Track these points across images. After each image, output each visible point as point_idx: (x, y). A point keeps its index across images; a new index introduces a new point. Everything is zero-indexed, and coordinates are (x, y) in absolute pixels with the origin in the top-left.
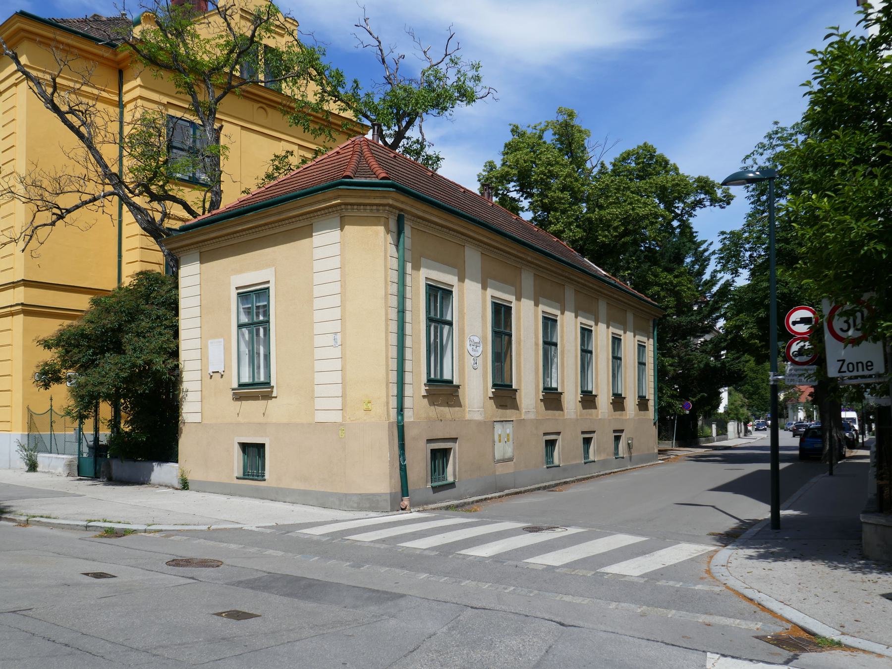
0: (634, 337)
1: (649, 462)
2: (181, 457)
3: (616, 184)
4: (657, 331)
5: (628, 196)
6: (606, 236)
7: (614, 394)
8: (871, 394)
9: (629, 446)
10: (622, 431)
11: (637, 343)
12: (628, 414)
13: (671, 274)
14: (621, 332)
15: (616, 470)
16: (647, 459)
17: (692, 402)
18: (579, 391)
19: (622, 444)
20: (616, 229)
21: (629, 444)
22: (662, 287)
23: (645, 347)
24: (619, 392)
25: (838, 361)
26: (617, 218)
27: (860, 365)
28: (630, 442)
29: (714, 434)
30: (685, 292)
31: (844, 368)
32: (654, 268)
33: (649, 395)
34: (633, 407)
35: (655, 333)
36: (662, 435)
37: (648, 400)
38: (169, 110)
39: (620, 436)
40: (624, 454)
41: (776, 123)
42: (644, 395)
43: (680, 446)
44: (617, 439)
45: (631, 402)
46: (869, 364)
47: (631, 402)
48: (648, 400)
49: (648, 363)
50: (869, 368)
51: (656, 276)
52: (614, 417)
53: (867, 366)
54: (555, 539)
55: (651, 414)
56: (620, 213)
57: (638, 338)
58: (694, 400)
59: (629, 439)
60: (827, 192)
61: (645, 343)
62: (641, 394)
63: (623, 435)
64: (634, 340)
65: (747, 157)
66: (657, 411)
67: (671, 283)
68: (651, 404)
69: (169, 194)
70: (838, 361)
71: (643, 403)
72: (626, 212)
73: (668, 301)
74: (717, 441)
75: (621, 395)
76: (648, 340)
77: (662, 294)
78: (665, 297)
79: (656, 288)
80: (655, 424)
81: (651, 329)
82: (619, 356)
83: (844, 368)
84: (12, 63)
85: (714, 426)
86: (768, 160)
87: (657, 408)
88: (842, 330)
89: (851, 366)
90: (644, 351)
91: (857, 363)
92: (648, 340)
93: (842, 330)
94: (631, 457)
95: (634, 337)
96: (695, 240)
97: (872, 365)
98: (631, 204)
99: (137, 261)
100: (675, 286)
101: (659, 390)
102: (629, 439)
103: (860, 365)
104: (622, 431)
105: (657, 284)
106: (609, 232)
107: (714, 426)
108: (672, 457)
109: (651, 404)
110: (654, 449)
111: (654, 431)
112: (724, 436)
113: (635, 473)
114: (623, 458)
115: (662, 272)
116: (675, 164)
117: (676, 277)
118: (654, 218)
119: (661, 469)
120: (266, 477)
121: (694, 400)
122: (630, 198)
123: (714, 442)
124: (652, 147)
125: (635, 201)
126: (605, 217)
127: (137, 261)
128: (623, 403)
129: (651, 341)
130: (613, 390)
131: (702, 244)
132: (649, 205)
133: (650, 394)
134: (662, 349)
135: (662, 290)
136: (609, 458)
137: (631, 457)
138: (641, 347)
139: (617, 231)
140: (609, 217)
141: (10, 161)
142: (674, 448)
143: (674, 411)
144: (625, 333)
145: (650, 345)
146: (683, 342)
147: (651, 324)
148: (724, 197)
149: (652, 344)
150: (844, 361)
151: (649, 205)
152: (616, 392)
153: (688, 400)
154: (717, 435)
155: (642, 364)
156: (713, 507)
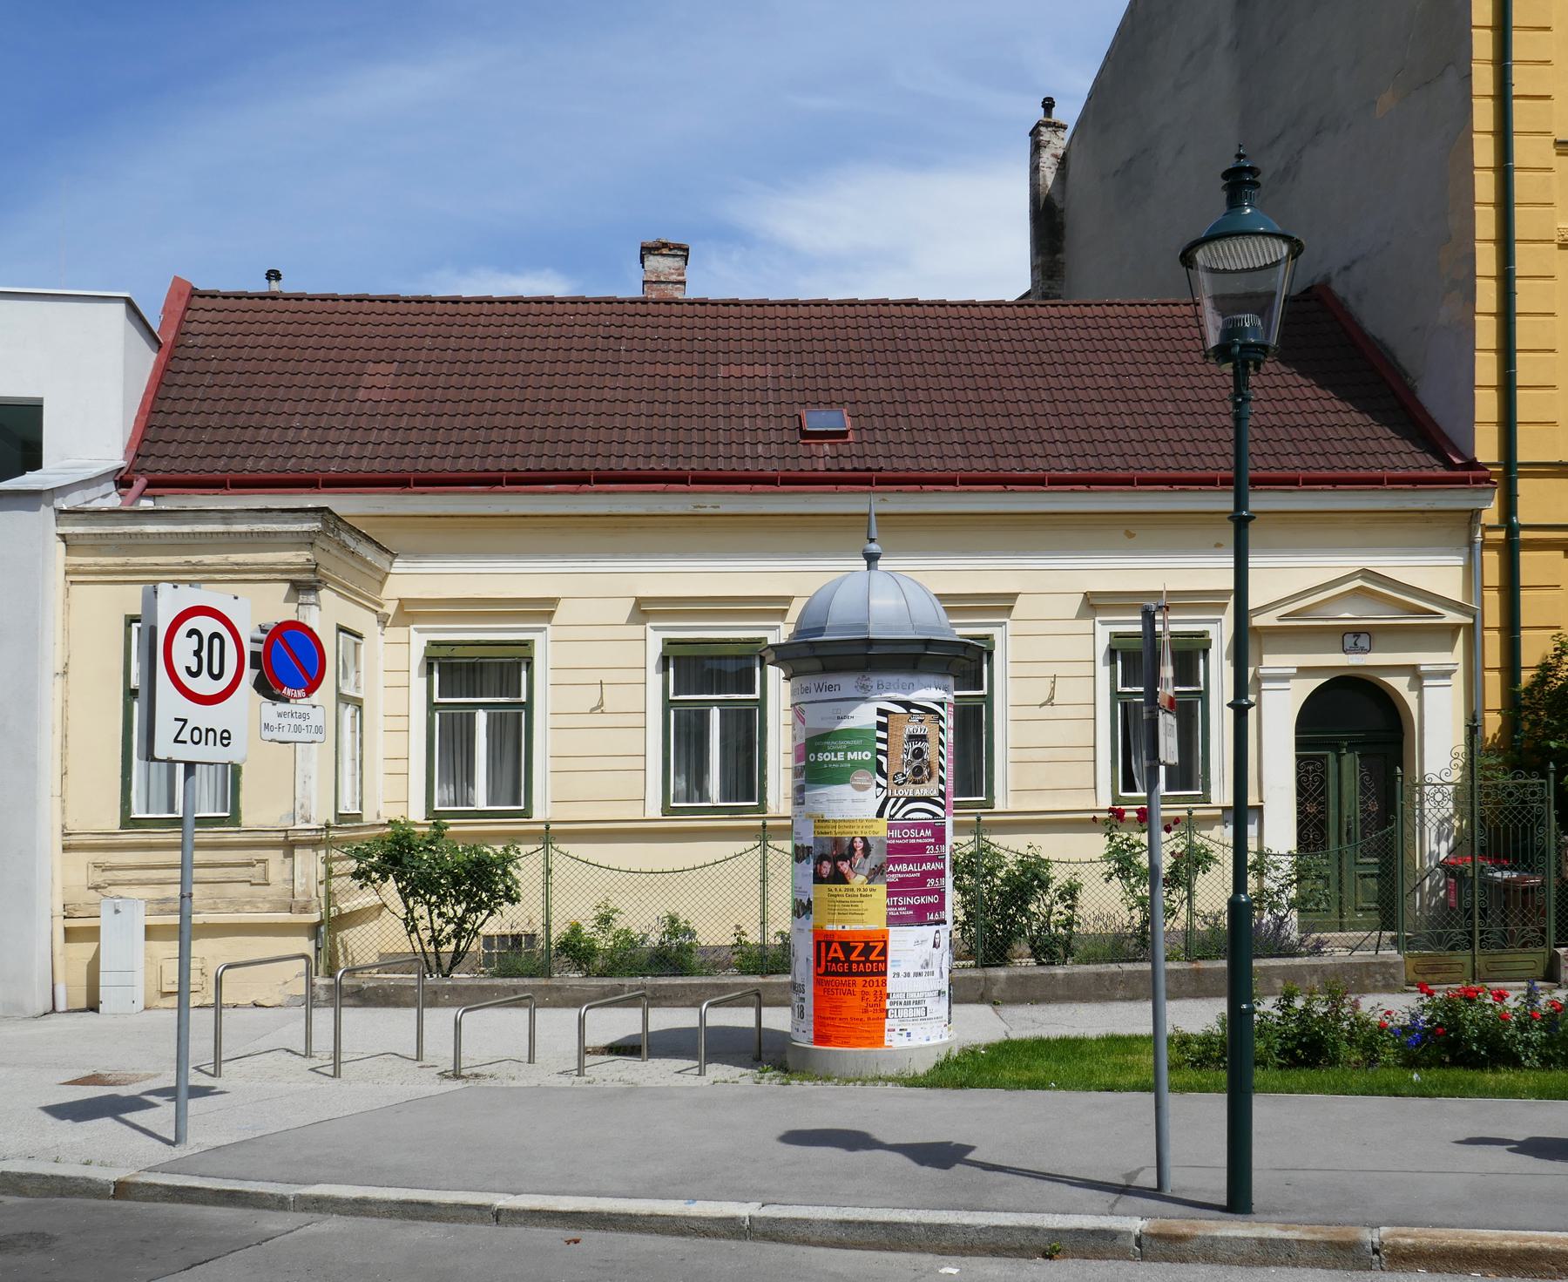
25: (176, 719)
27: (211, 734)
31: (185, 736)
41: (1240, 156)
46: (225, 735)
50: (225, 742)
53: (222, 738)
54: (100, 1099)
60: (1200, 703)
69: (133, 704)
70: (176, 719)
83: (185, 736)
84: (174, 940)
88: (188, 669)
89: (196, 733)
91: (208, 731)
93: (188, 669)
97: (229, 738)
99: (1552, 241)
103: (211, 734)
127: (1552, 241)
141: (547, 895)
150: (185, 721)
156: (288, 1051)
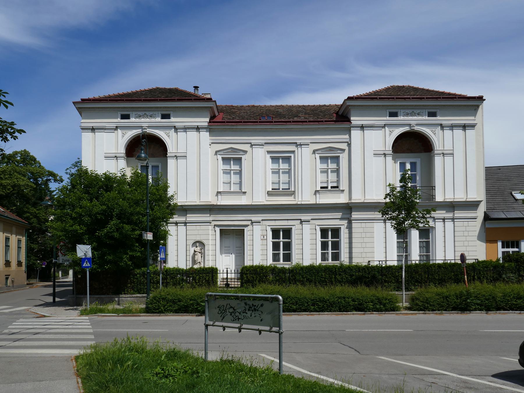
0: (16, 236)
1: (22, 288)
2: (501, 252)
3: (9, 170)
4: (27, 234)
5: (15, 175)
6: (3, 192)
7: (6, 261)
8: (426, 215)
9: (13, 282)
10: (9, 275)
11: (17, 239)
12: (12, 269)
13: (35, 209)
14: (9, 235)
15: (6, 291)
16: (21, 287)
17: (47, 262)
18: (17, 261)
19: (9, 281)
20: (9, 189)
21: (12, 280)
22: (31, 214)
23: (21, 240)
24: (8, 260)
26: (10, 184)
28: (13, 280)
29: (60, 276)
30: (41, 217)
32: (27, 205)
33: (22, 260)
34: (15, 266)
35: (26, 235)
36: (29, 277)
37: (22, 262)
38: (92, 332)
39: (8, 277)
40: (10, 285)
42: (20, 260)
43: (41, 282)
44: (7, 279)
45: (14, 264)
47: (14, 264)
48: (22, 262)
49: (22, 247)
51: (28, 209)
52: (5, 270)
55: (24, 268)
56: (11, 183)
57: (18, 237)
58: (48, 261)
59: (12, 279)
61: (21, 239)
62: (19, 260)
63: (10, 277)
64: (16, 238)
65: (68, 169)
66: (26, 267)
67: (35, 212)
68: (24, 264)
71: (19, 264)
72: (14, 182)
73: (33, 220)
74: (62, 279)
75: (9, 261)
76: (23, 237)
77: (31, 217)
78: (32, 218)
79: (28, 214)
80: (25, 272)
81: (24, 233)
82: (8, 245)
85: (60, 272)
86: (76, 171)
87: (26, 265)
90: (20, 243)
92: (23, 237)
94: (13, 286)
95: (16, 236)
96: (50, 190)
98: (17, 178)
100: (37, 214)
101: (28, 257)
102: (12, 279)
104: (9, 275)
105: (29, 213)
106: (5, 190)
107: (60, 272)
108: (35, 286)
109: (24, 264)
110: (25, 283)
111: (25, 275)
112: (66, 277)
113: (15, 292)
114: (10, 286)
115: (31, 207)
116: (39, 161)
117: (37, 210)
118: (27, 186)
119: (28, 290)
120: (320, 242)
121: (48, 261)
122: (16, 176)
123: (60, 279)
124: (28, 152)
125: (19, 178)
126: (3, 184)
128: (10, 264)
129: (24, 238)
130: (5, 259)
131: (54, 192)
132: (25, 180)
133: (23, 259)
134: (31, 239)
135: (31, 215)
136: (3, 286)
137: (13, 286)
138: (19, 241)
139: (9, 191)
140: (5, 184)
142: (37, 282)
143: (36, 266)
144: (11, 235)
145: (24, 240)
146: (42, 236)
147: (24, 231)
148: (60, 179)
149: (25, 239)
150: (63, 259)
151: (25, 180)
152: (7, 260)
153: (45, 261)
154: (62, 276)
155: (19, 248)
